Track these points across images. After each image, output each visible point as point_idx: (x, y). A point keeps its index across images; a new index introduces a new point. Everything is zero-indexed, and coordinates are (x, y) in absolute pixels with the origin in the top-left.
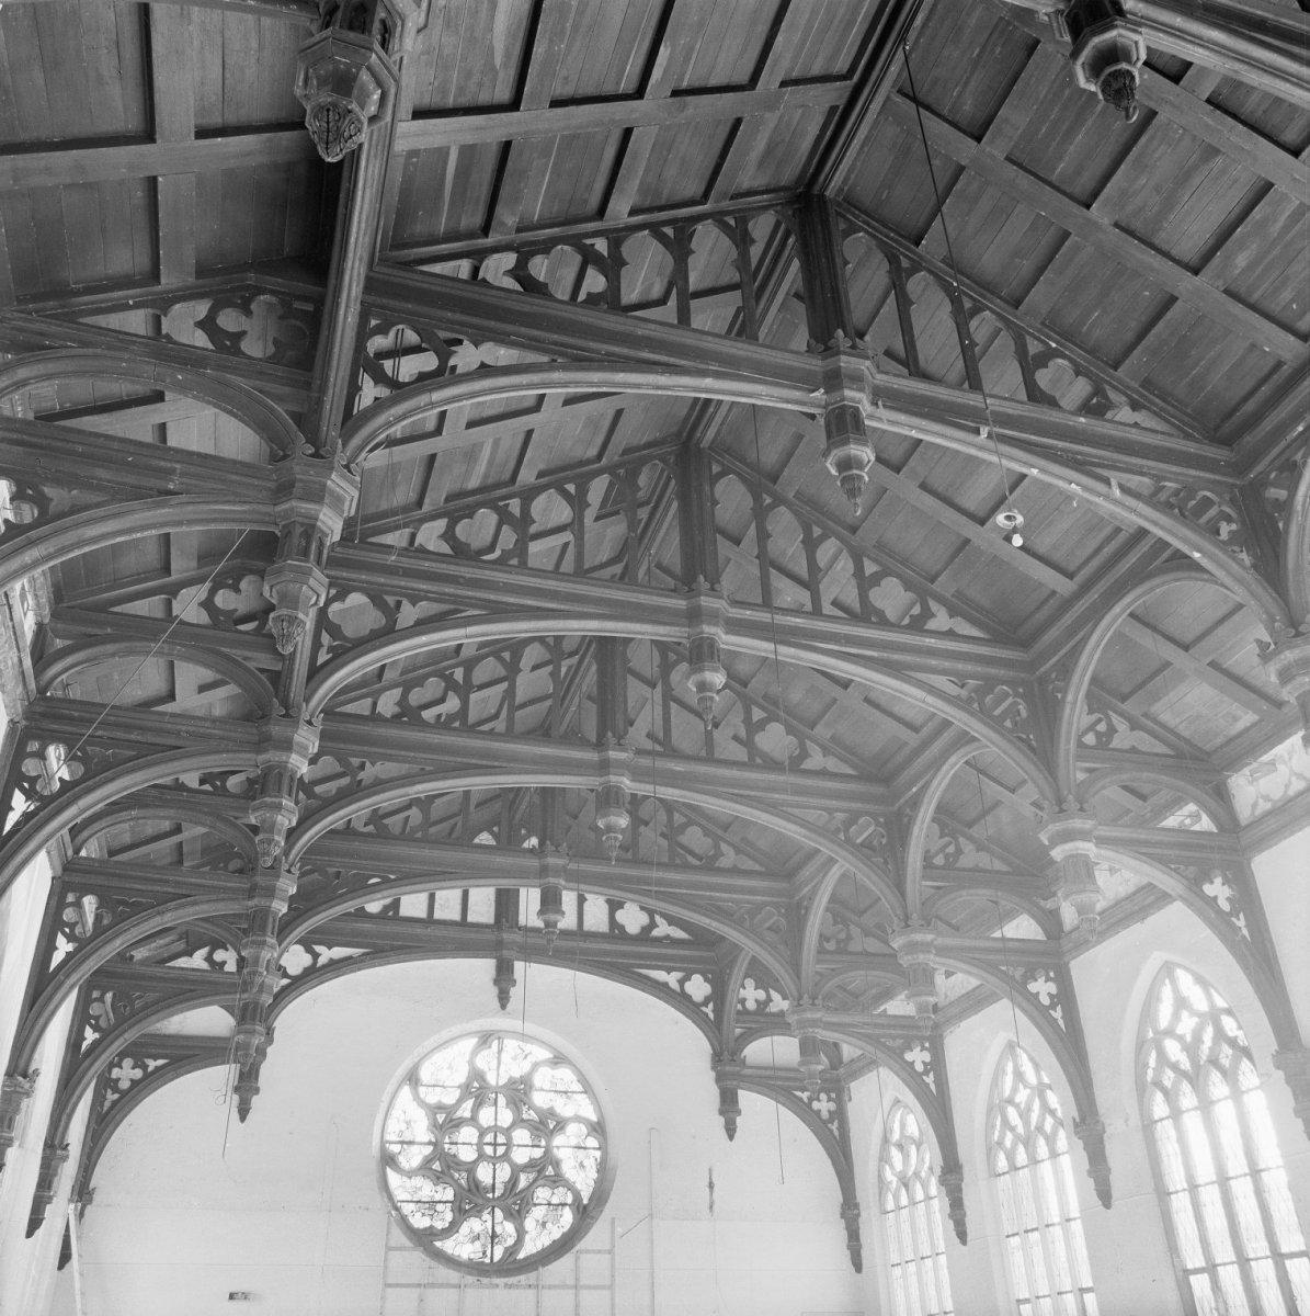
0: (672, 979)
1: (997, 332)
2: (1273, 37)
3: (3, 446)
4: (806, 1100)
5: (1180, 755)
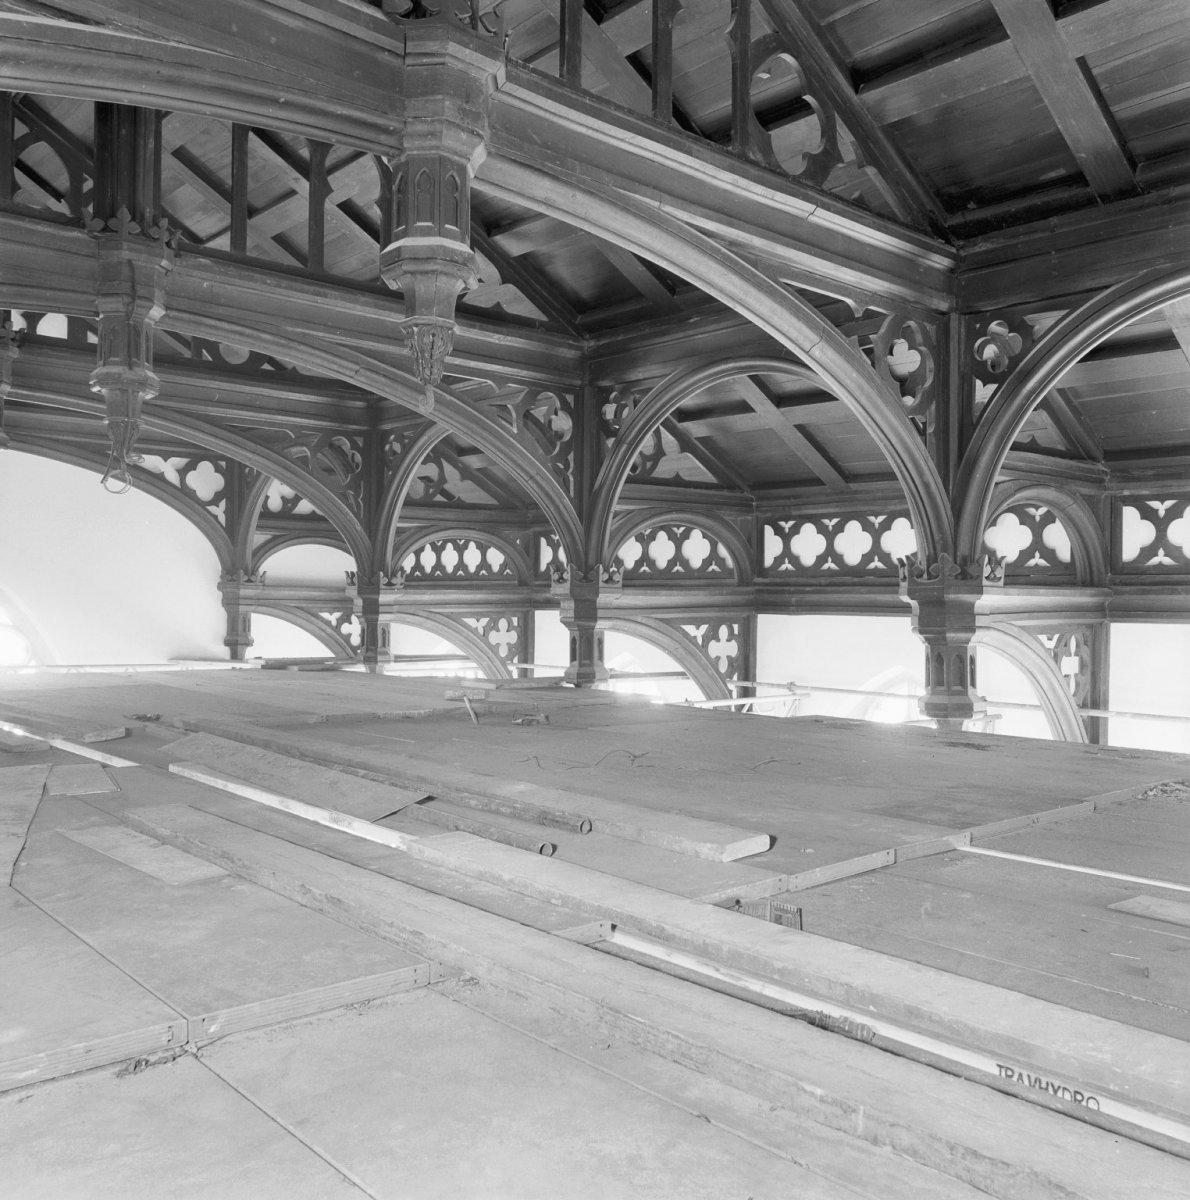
0: (169, 468)
1: (1186, 149)
2: (1123, 302)
3: (4, 289)
4: (334, 623)
5: (506, 506)
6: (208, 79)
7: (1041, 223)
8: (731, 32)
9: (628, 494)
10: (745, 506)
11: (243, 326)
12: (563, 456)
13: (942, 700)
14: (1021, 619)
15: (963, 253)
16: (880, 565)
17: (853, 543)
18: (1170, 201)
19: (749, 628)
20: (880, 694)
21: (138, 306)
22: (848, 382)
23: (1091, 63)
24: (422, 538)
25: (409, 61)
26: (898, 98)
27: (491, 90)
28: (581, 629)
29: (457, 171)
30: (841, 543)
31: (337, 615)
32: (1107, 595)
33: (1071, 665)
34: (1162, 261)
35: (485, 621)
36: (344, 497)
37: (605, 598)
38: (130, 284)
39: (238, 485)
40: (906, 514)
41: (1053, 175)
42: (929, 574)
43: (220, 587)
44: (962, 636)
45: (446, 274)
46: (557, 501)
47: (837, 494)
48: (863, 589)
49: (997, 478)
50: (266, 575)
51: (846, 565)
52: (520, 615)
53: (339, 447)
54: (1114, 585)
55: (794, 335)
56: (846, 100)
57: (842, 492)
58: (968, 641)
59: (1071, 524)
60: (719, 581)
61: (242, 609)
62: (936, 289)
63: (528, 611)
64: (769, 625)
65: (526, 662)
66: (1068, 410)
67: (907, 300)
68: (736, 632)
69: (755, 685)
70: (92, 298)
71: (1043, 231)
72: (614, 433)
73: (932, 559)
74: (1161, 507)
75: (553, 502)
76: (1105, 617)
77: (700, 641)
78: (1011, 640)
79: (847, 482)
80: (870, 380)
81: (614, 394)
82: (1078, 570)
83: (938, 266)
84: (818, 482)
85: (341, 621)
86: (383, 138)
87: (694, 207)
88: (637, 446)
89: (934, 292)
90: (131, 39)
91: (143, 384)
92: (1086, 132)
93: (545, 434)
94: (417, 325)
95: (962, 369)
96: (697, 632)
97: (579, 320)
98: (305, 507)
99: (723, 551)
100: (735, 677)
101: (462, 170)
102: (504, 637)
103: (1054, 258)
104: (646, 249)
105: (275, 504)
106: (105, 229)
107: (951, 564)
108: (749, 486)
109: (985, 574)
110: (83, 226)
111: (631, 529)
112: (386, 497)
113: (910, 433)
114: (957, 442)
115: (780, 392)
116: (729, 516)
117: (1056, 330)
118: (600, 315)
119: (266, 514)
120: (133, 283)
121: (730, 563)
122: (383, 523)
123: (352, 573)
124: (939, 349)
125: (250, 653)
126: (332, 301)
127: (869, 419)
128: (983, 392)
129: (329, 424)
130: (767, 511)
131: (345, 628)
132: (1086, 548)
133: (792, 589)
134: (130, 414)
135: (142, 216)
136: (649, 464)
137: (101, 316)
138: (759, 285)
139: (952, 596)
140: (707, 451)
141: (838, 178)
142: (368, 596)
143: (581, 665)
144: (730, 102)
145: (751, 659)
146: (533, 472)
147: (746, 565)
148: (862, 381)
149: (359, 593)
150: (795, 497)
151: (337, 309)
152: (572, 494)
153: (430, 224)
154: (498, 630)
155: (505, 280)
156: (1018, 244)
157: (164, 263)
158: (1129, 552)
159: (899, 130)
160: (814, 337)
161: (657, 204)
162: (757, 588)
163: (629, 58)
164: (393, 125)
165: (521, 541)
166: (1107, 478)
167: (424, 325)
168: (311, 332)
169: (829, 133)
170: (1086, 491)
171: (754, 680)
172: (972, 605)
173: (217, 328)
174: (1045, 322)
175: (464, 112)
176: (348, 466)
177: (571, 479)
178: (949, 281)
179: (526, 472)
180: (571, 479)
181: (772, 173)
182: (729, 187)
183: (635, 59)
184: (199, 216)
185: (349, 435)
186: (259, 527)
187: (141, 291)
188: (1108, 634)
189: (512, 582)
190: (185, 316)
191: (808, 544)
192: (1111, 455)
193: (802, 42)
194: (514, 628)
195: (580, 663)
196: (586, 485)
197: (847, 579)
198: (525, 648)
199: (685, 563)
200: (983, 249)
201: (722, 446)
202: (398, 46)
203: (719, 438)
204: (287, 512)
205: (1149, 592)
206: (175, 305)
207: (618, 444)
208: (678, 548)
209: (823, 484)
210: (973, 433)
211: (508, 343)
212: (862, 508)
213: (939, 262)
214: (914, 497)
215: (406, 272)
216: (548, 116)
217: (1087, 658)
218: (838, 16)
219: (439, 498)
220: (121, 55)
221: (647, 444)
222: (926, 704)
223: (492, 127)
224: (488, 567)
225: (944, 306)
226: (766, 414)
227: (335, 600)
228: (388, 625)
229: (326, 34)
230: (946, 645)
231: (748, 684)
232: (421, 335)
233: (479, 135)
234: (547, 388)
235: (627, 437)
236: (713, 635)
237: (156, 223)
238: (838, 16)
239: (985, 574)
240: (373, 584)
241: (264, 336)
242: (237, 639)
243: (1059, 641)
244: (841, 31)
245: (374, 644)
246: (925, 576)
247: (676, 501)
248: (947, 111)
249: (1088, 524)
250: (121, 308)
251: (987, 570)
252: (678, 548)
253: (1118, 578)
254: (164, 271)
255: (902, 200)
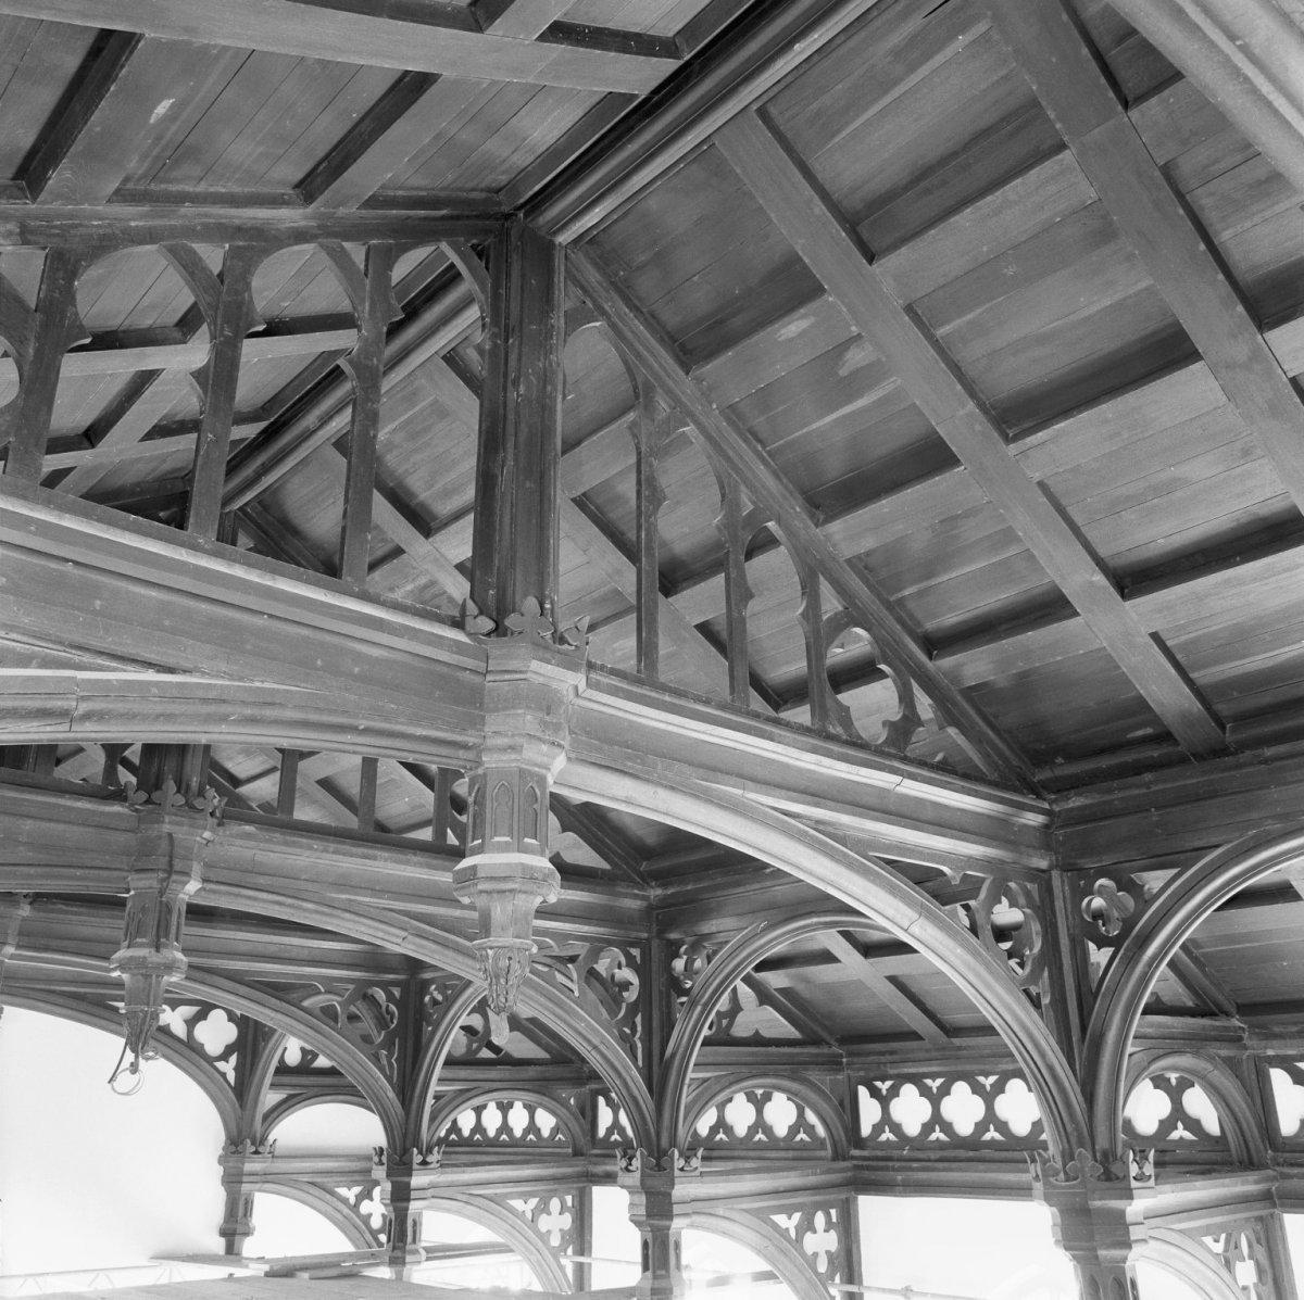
6: (290, 714)
7: (1136, 779)
8: (802, 614)
9: (702, 1060)
10: (833, 1064)
11: (284, 895)
12: (629, 1020)
14: (1180, 1221)
15: (1057, 808)
16: (997, 1136)
17: (963, 1109)
18: (1266, 761)
19: (849, 1212)
21: (174, 882)
22: (952, 959)
23: (1164, 636)
24: (464, 1102)
25: (489, 678)
26: (975, 665)
27: (572, 695)
28: (655, 1230)
29: (537, 782)
30: (949, 1107)
31: (357, 1190)
32: (1274, 1179)
33: (1246, 1272)
34: (1270, 821)
35: (533, 1202)
36: (376, 1059)
37: (681, 1190)
38: (167, 858)
39: (251, 1041)
40: (1019, 1074)
41: (1140, 733)
42: (1066, 1173)
43: (222, 1160)
44: (1116, 1253)
45: (525, 892)
46: (624, 1074)
47: (938, 1050)
48: (981, 1166)
49: (1130, 1049)
50: (277, 1143)
52: (574, 1192)
53: (372, 996)
54: (1278, 1164)
55: (890, 912)
56: (920, 666)
57: (944, 1049)
58: (1124, 1260)
59: (1214, 1091)
60: (811, 1154)
61: (245, 1187)
62: (1034, 847)
63: (584, 1187)
64: (871, 1209)
65: (582, 1254)
66: (1195, 964)
67: (1004, 861)
68: (834, 1220)
69: (862, 1291)
70: (125, 874)
71: (1138, 787)
72: (686, 992)
75: (620, 1075)
76: (1274, 1206)
77: (793, 1234)
78: (1174, 1250)
79: (948, 1036)
80: (975, 954)
81: (685, 947)
82: (1232, 1145)
83: (1031, 823)
84: (914, 1036)
85: (360, 1198)
86: (461, 753)
87: (778, 791)
88: (714, 1005)
89: (1031, 851)
90: (215, 685)
91: (170, 967)
92: (1167, 695)
93: (607, 991)
94: (491, 948)
95: (1072, 931)
96: (789, 1222)
97: (644, 866)
98: (322, 1062)
99: (811, 1117)
100: (837, 1279)
101: (542, 780)
102: (557, 1221)
103: (1154, 815)
104: (730, 838)
105: (293, 1057)
106: (148, 802)
107: (1091, 1163)
108: (837, 1040)
109: (1133, 1174)
110: (125, 799)
111: (710, 1099)
112: (425, 1057)
113: (1024, 1008)
114: (1078, 1016)
115: (866, 939)
116: (814, 1075)
117: (1169, 892)
118: (665, 864)
119: (283, 1069)
120: (171, 857)
121: (821, 1131)
122: (418, 1091)
123: (381, 1149)
124: (1044, 910)
125: (249, 1247)
126: (381, 863)
127: (979, 996)
128: (1099, 956)
129: (363, 974)
130: (859, 1070)
131: (366, 1207)
132: (1237, 1121)
133: (897, 1164)
134: (151, 1002)
135: (188, 786)
136: (725, 1022)
137: (132, 893)
138: (850, 865)
139: (1098, 1203)
140: (790, 1004)
141: (921, 739)
142: (399, 1179)
143: (655, 1277)
144: (805, 664)
145: (854, 1250)
146: (596, 1041)
147: (841, 1134)
148: (969, 958)
149: (388, 1176)
150: (892, 1053)
151: (387, 871)
152: (640, 1063)
153: (508, 839)
154: (549, 1214)
155: (565, 829)
156: (1114, 800)
157: (207, 834)
159: (979, 694)
160: (913, 915)
161: (739, 792)
162: (855, 1162)
163: (697, 627)
164: (471, 740)
165: (576, 1100)
166: (1246, 1035)
167: (499, 947)
168: (358, 898)
169: (906, 699)
170: (1224, 1053)
171: (860, 1283)
172: (1122, 1214)
173: (255, 899)
174: (1154, 880)
175: (545, 725)
176: (382, 1022)
177: (639, 1045)
178: (1045, 838)
179: (589, 1041)
180: (639, 1045)
181: (855, 745)
182: (812, 767)
183: (705, 629)
184: (241, 758)
185: (385, 986)
186: (273, 1086)
187: (178, 865)
188: (1282, 1227)
189: (565, 1150)
190: (222, 888)
191: (911, 1110)
192: (1247, 1009)
193: (872, 614)
194: (568, 1210)
195: (654, 1272)
196: (656, 1052)
197: (962, 1153)
198: (581, 1235)
199: (768, 1130)
200: (1078, 804)
201: (804, 996)
202: (482, 666)
203: (800, 988)
204: (305, 1068)
206: (213, 877)
207: (693, 1004)
208: (760, 1112)
209: (922, 1039)
210: (1095, 1003)
211: (569, 897)
212: (968, 1067)
213: (1034, 819)
214: (1037, 1080)
215: (481, 892)
216: (627, 716)
217: (1265, 1262)
218: (906, 593)
219: (486, 1053)
220: (205, 701)
221: (723, 1004)
223: (571, 732)
224: (537, 1132)
225: (1043, 864)
226: (852, 964)
227: (354, 1172)
228: (420, 1214)
229: (408, 659)
230: (1100, 1265)
231: (853, 1288)
232: (496, 958)
233: (559, 746)
234: (610, 943)
235: (702, 997)
236: (807, 1226)
237: (201, 793)
238: (906, 593)
239: (1133, 1174)
240: (405, 1164)
241: (305, 905)
242: (235, 1226)
243: (1227, 1241)
244: (911, 605)
245: (400, 1235)
246: (1062, 1175)
247: (758, 1061)
248: (1023, 676)
249: (1233, 1090)
250: (155, 884)
251: (1134, 1169)
252: (760, 1112)
253: (1281, 1157)
254: (205, 842)
255: (986, 756)
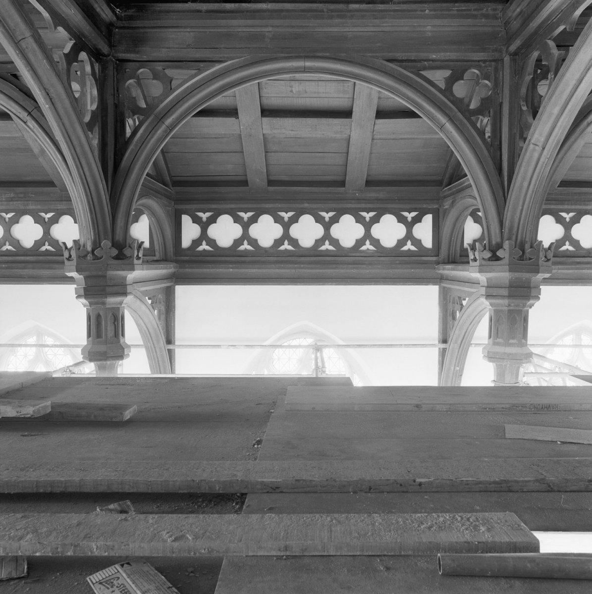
13: (103, 348)
20: (13, 345)
44: (118, 299)
51: (22, 247)
73: (96, 245)
74: (567, 216)
158: (186, 242)
172: (125, 278)
191: (225, 231)
205: (12, 268)
208: (47, 232)
222: (89, 352)
252: (47, 232)
